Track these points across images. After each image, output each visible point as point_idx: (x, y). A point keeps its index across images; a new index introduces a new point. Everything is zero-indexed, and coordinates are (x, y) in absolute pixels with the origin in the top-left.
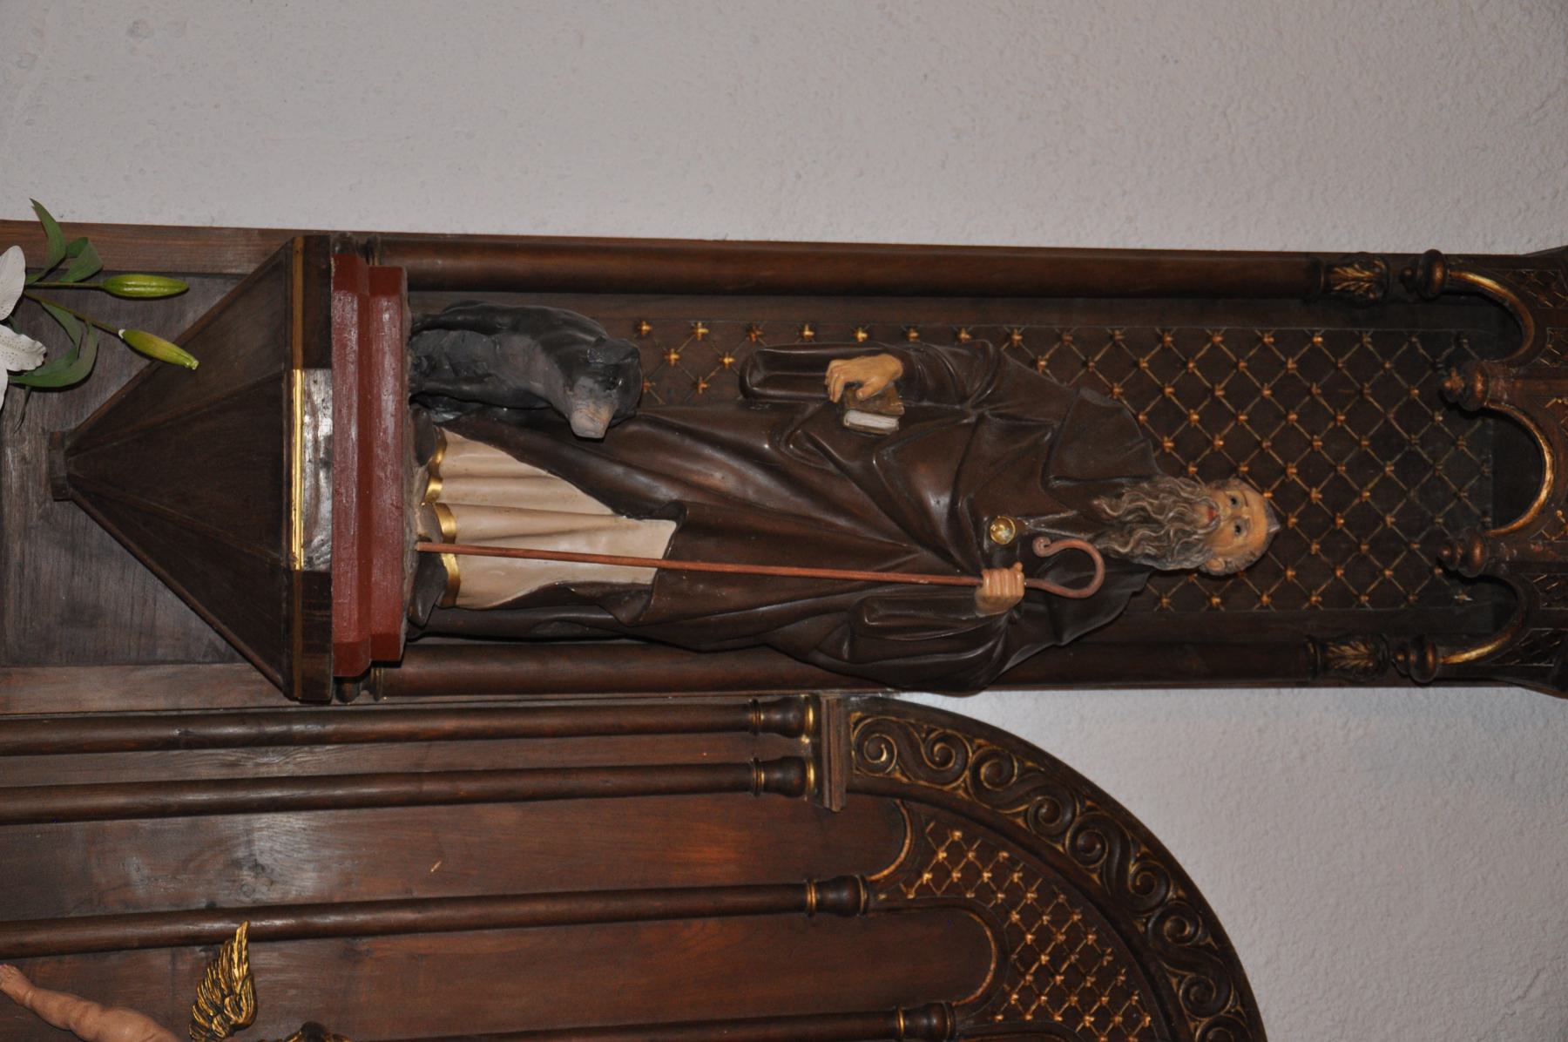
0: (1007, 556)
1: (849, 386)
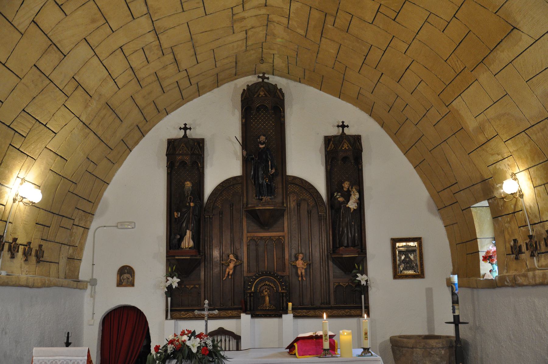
0: (190, 204)
1: (177, 216)
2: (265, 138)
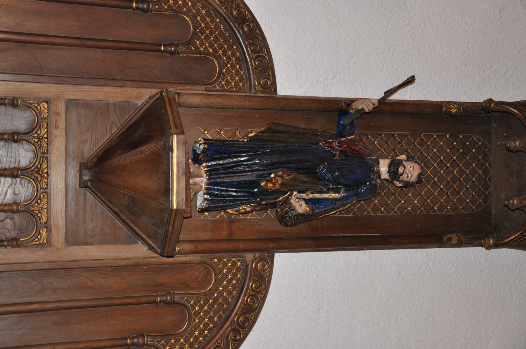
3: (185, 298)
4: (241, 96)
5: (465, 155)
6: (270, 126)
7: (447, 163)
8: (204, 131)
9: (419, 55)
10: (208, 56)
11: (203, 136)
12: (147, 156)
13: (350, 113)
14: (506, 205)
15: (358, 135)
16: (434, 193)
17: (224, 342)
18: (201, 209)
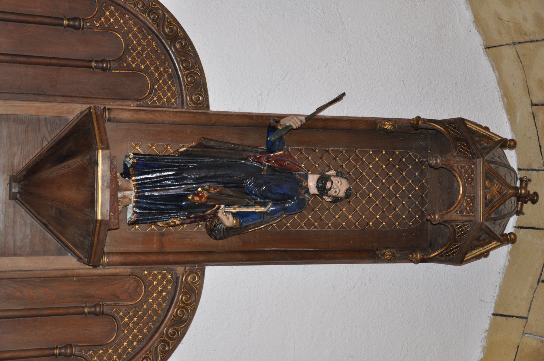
2: (342, 194)
3: (114, 310)
4: (172, 111)
5: (401, 171)
6: (201, 141)
7: (383, 179)
8: (136, 146)
9: (356, 71)
10: (140, 73)
11: (134, 151)
12: (74, 169)
13: (277, 129)
14: (428, 219)
15: (287, 151)
16: (369, 209)
17: (153, 353)
18: (131, 222)
